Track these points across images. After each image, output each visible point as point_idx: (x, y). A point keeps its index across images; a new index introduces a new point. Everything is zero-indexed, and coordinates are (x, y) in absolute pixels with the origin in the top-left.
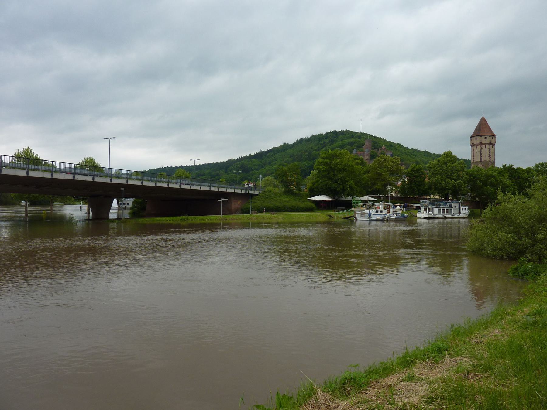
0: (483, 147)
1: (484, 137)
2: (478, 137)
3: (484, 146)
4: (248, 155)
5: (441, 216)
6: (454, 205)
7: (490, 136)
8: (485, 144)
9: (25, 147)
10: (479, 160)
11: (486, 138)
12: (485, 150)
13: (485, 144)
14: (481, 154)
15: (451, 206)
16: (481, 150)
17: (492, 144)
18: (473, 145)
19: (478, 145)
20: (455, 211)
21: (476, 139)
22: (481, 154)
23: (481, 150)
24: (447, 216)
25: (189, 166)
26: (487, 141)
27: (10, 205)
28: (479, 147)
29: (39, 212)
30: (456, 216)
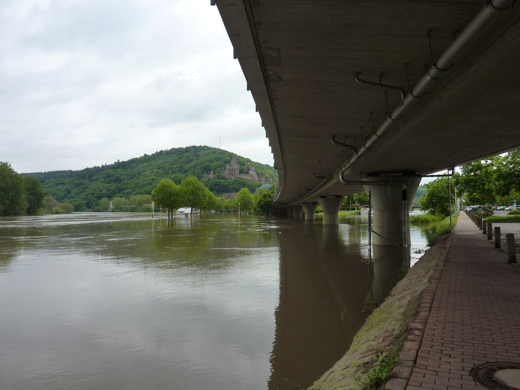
9: (140, 156)
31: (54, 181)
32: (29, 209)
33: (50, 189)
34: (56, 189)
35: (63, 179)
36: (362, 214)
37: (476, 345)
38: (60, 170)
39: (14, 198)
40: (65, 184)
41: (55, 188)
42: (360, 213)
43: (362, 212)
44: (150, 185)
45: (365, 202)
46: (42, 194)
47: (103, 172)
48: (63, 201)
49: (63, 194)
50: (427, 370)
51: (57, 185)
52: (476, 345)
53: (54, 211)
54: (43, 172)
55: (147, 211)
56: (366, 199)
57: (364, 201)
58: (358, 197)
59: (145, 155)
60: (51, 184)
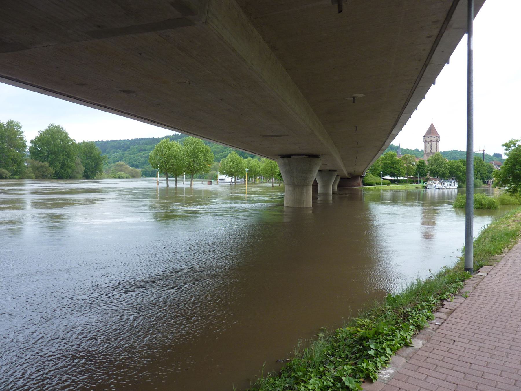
0: (433, 143)
1: (433, 137)
2: (429, 137)
3: (428, 143)
4: (77, 143)
5: (448, 187)
6: (453, 182)
7: (437, 136)
8: (433, 142)
9: (10, 119)
10: (430, 152)
11: (434, 137)
12: (434, 145)
13: (433, 142)
14: (431, 148)
15: (451, 182)
16: (431, 145)
17: (437, 141)
18: (425, 142)
19: (429, 142)
20: (453, 185)
21: (428, 138)
22: (431, 148)
23: (431, 145)
24: (451, 187)
25: (449, 151)
26: (435, 140)
27: (67, 178)
28: (430, 143)
29: (259, 195)
30: (453, 187)
31: (137, 148)
32: (85, 172)
33: (133, 155)
34: (138, 155)
35: (145, 145)
36: (428, 188)
37: (489, 327)
38: (145, 137)
39: (66, 161)
40: (146, 151)
41: (137, 154)
42: (426, 187)
43: (429, 186)
44: (222, 153)
45: (439, 174)
46: (100, 158)
47: (181, 139)
48: (143, 166)
49: (143, 160)
50: (494, 346)
51: (140, 151)
52: (489, 327)
53: (117, 176)
54: (130, 139)
55: (214, 178)
56: (440, 170)
57: (437, 173)
58: (430, 168)
59: (406, 124)
60: (135, 150)
